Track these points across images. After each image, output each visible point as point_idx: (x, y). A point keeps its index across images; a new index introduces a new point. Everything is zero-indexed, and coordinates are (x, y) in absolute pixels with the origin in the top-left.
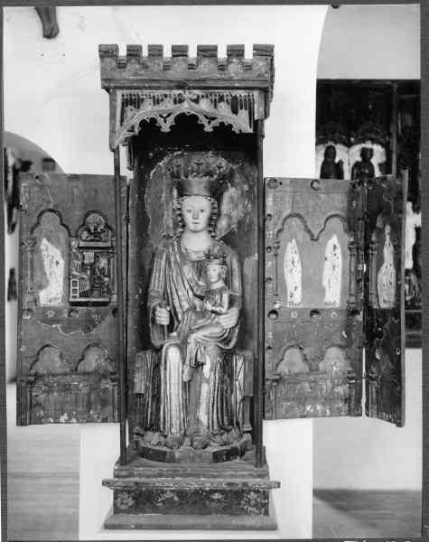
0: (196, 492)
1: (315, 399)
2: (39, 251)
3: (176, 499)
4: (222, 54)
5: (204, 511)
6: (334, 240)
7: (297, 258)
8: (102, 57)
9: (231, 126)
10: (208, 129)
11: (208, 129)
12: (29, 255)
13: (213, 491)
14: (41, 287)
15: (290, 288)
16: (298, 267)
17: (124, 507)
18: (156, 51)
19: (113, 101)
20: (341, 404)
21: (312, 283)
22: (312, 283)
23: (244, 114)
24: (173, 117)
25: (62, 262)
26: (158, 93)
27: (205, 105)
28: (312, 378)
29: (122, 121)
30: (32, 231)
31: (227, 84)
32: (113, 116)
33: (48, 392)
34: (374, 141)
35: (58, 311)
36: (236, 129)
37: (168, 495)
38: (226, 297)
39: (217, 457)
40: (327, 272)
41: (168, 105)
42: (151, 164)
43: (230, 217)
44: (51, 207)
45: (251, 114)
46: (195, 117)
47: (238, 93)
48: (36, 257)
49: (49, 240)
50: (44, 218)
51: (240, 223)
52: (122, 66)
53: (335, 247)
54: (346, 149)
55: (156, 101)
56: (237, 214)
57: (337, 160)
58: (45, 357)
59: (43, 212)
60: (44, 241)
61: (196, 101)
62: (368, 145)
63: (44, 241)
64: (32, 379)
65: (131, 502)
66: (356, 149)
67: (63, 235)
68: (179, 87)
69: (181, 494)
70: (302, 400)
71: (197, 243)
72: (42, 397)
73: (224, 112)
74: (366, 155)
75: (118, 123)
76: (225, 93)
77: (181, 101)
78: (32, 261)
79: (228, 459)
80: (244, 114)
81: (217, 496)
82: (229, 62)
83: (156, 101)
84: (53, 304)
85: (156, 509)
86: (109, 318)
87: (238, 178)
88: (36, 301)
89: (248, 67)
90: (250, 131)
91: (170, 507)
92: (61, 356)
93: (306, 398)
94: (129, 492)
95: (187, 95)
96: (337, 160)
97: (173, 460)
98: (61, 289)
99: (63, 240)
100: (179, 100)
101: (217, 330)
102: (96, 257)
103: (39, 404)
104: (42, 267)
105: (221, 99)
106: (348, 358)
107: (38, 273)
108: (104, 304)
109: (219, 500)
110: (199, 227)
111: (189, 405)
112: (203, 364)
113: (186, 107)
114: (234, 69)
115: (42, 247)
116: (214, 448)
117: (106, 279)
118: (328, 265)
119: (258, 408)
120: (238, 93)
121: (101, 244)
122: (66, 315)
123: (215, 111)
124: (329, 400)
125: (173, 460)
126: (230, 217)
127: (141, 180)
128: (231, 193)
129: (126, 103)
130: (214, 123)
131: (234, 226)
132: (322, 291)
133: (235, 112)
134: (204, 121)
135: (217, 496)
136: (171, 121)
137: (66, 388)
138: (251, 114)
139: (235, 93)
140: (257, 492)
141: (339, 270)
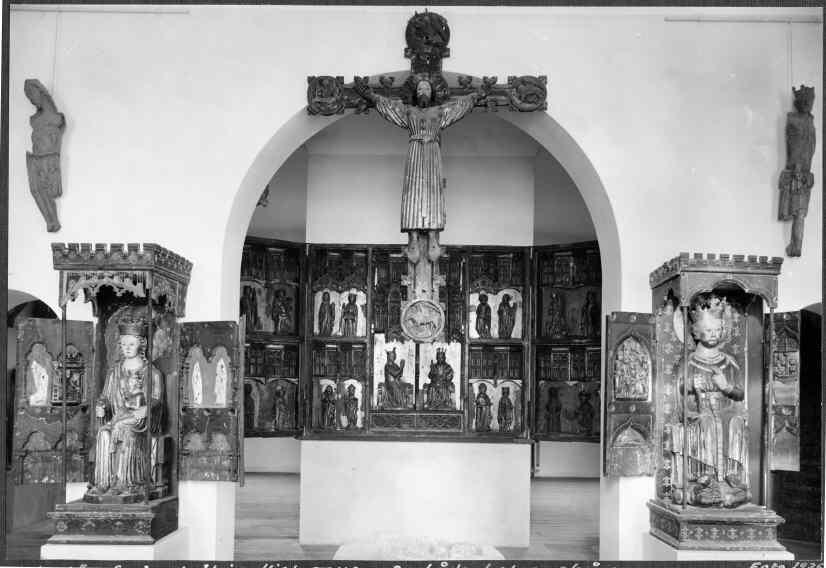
0: (106, 521)
1: (210, 468)
2: (31, 369)
3: (94, 525)
4: (126, 249)
5: (111, 533)
6: (221, 362)
7: (199, 374)
8: (54, 251)
9: (132, 293)
10: (119, 294)
11: (119, 294)
12: (24, 373)
13: (116, 521)
14: (31, 394)
15: (196, 396)
16: (200, 380)
17: (60, 530)
18: (86, 247)
19: (61, 277)
20: (227, 473)
21: (208, 390)
22: (208, 390)
23: (140, 285)
24: (98, 287)
25: (47, 377)
26: (89, 273)
27: (116, 281)
28: (207, 454)
29: (67, 288)
30: (26, 355)
31: (127, 267)
32: (61, 286)
33: (35, 463)
34: (358, 289)
35: (44, 409)
36: (135, 294)
37: (90, 523)
38: (138, 398)
39: (126, 500)
40: (218, 384)
41: (95, 280)
42: (109, 314)
43: (159, 349)
44: (40, 340)
45: (144, 285)
46: (111, 288)
47: (137, 273)
48: (28, 373)
49: (38, 362)
50: (34, 347)
51: (165, 352)
52: (65, 256)
53: (222, 367)
54: (338, 294)
55: (88, 278)
56: (163, 346)
57: (331, 303)
58: (33, 439)
59: (35, 343)
60: (35, 363)
61: (112, 277)
62: (354, 291)
63: (35, 363)
64: (24, 454)
65: (66, 527)
66: (346, 294)
67: (48, 360)
68: (100, 269)
69: (97, 522)
70: (203, 469)
71: (134, 364)
72: (30, 466)
73: (128, 284)
74: (352, 299)
75: (64, 290)
76: (129, 272)
77: (103, 278)
78: (25, 376)
79: (135, 502)
80: (140, 285)
81: (118, 523)
82: (129, 254)
83: (88, 278)
84: (39, 404)
85: (81, 532)
86: (80, 413)
87: (164, 323)
88: (28, 402)
89: (140, 257)
90: (143, 295)
91: (90, 531)
92: (45, 439)
93: (84, 454)
94: (64, 521)
95: (106, 274)
96: (331, 303)
97: (98, 502)
98: (45, 394)
99: (48, 363)
100: (101, 277)
101: (131, 421)
102: (71, 375)
103: (27, 471)
104: (33, 379)
105: (127, 276)
106: (228, 441)
107: (29, 384)
108: (76, 404)
109: (120, 526)
110: (131, 355)
111: (112, 470)
112: (121, 442)
113: (105, 281)
114: (132, 258)
115: (33, 367)
116: (126, 494)
117: (78, 388)
118: (218, 378)
119: (171, 469)
120: (137, 273)
121: (75, 365)
122: (49, 412)
123: (133, 286)
124: (218, 470)
125: (98, 502)
126: (159, 349)
127: (103, 325)
128: (160, 332)
129: (70, 278)
130: (123, 291)
131: (160, 354)
132: (215, 397)
133: (135, 283)
134: (116, 290)
135: (118, 523)
136: (97, 290)
137: (48, 460)
138: (144, 285)
139: (135, 272)
140: (143, 520)
141: (225, 382)
